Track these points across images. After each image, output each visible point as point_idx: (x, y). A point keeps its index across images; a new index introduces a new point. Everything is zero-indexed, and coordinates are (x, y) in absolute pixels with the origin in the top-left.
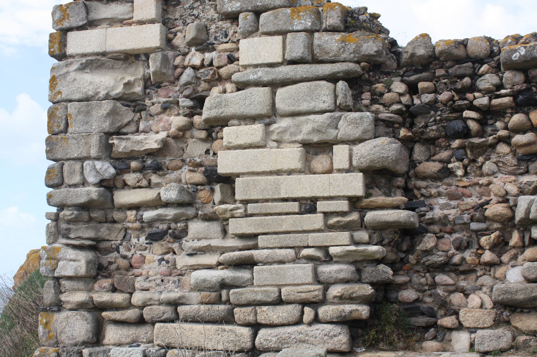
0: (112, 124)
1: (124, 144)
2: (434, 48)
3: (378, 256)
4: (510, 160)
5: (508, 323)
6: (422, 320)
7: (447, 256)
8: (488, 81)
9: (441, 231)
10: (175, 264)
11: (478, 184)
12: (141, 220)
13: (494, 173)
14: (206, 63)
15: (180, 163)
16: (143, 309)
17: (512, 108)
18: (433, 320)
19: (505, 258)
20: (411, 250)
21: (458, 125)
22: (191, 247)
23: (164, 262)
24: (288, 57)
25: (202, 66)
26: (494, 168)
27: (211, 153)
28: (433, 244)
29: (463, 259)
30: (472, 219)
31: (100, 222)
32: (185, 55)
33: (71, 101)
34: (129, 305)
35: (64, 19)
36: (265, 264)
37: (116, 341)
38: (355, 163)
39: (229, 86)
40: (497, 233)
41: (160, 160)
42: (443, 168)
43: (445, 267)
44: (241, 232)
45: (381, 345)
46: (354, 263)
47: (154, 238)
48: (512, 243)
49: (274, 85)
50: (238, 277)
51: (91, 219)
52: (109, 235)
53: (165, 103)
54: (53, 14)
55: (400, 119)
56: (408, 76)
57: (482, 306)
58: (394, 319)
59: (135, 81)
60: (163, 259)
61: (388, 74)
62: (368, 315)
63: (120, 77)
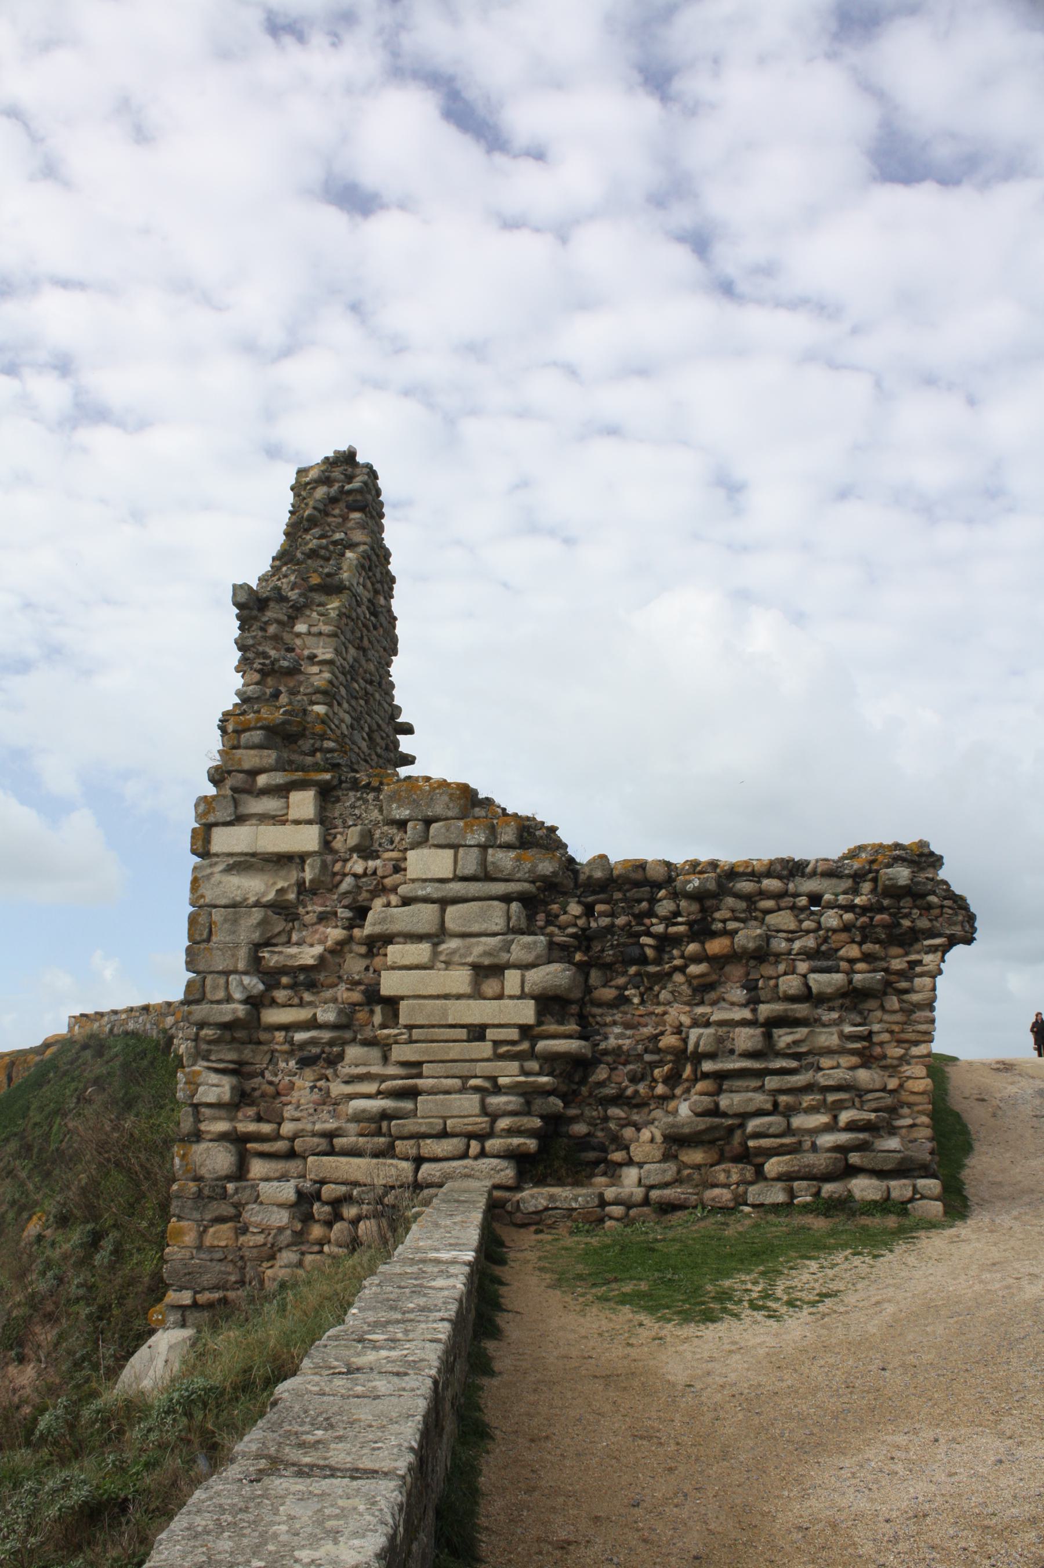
0: (261, 935)
1: (276, 958)
2: (612, 870)
3: (548, 1088)
4: (685, 989)
5: (676, 1157)
6: (592, 1155)
7: (620, 1089)
8: (665, 907)
9: (614, 1062)
10: (328, 1092)
11: (653, 1013)
12: (291, 1042)
13: (669, 1003)
14: (369, 872)
15: (336, 980)
16: (293, 1141)
17: (688, 937)
18: (603, 1155)
19: (678, 1091)
20: (583, 1081)
21: (635, 951)
22: (346, 1075)
23: (316, 1090)
24: (459, 873)
25: (365, 874)
26: (669, 997)
27: (371, 970)
28: (605, 1076)
29: (636, 1092)
30: (646, 1051)
31: (243, 1043)
32: (346, 861)
33: (216, 906)
34: (277, 1137)
35: (209, 812)
36: (429, 1094)
37: (264, 1175)
38: (526, 990)
39: (394, 899)
40: (670, 1065)
41: (314, 976)
42: (619, 995)
43: (619, 1099)
44: (405, 1059)
45: (549, 1180)
46: (523, 1094)
47: (305, 1062)
48: (685, 1076)
49: (444, 903)
50: (401, 1108)
51: (234, 1040)
52: (253, 1057)
53: (321, 913)
54: (196, 806)
55: (576, 943)
56: (585, 897)
57: (652, 1140)
58: (562, 1153)
59: (289, 886)
60: (315, 1087)
61: (565, 894)
62: (536, 1149)
63: (271, 882)
